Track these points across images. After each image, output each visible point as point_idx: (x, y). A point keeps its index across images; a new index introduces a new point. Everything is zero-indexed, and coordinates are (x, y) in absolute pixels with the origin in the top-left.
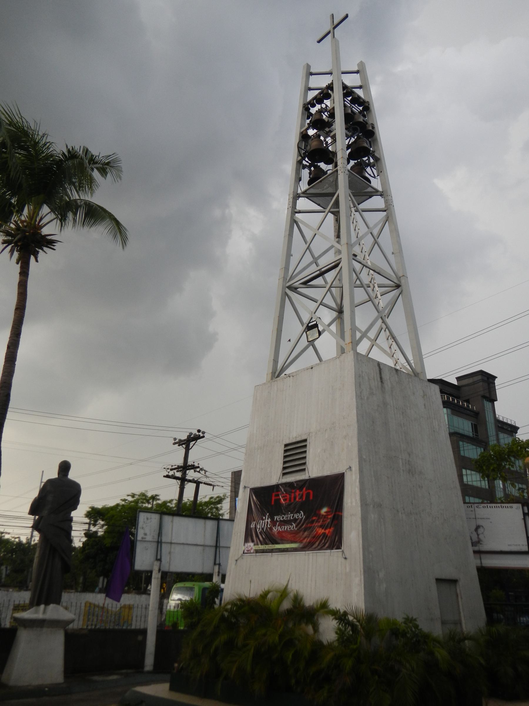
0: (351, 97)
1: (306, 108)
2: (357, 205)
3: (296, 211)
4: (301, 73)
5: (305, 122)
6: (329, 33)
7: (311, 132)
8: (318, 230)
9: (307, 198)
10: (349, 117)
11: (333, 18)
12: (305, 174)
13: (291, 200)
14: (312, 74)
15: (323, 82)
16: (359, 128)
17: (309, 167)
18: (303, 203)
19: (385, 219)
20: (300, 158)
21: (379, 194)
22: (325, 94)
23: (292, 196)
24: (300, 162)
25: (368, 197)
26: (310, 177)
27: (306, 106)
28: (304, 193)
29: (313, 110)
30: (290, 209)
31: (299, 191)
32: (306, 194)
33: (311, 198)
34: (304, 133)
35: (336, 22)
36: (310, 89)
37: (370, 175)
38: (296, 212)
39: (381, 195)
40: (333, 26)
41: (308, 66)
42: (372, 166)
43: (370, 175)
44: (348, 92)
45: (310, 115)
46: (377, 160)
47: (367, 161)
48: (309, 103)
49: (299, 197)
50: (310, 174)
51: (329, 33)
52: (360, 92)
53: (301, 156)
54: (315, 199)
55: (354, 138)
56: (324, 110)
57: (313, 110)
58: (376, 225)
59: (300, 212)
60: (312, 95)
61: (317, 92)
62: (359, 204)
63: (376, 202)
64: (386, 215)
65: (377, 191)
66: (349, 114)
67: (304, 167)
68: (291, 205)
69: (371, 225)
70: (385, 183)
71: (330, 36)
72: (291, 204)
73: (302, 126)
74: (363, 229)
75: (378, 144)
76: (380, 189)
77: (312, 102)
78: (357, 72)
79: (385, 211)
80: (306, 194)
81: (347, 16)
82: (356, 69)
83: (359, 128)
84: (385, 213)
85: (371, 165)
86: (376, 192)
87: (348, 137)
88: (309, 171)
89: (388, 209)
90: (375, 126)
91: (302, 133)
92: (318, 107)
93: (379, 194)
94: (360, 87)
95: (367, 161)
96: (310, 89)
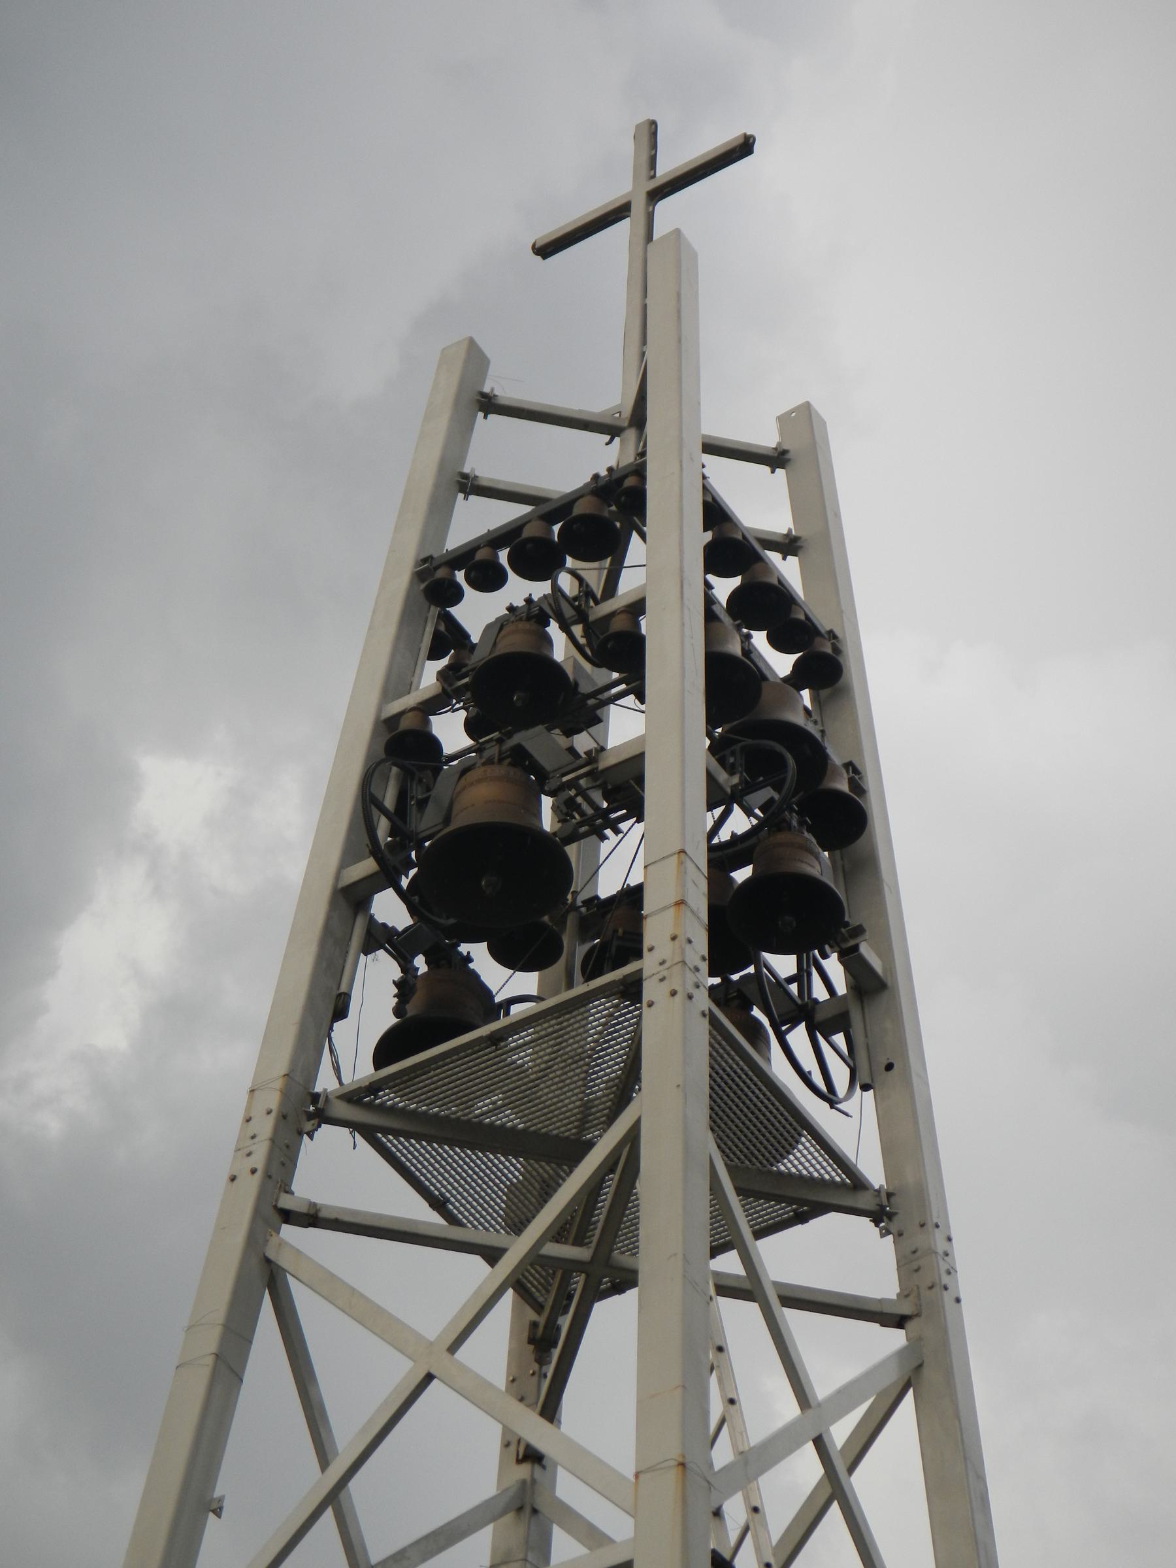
0: (736, 581)
1: (435, 585)
2: (747, 1232)
3: (285, 1202)
4: (429, 393)
5: (414, 669)
6: (619, 213)
7: (451, 731)
8: (454, 1348)
9: (368, 1133)
10: (730, 686)
11: (654, 145)
12: (376, 985)
13: (265, 1127)
14: (489, 405)
15: (569, 465)
16: (791, 761)
17: (400, 946)
18: (341, 1168)
19: (892, 1377)
20: (368, 866)
21: (864, 1201)
22: (606, 517)
23: (272, 1100)
24: (352, 899)
25: (786, 1211)
26: (398, 1011)
27: (441, 573)
28: (354, 1097)
29: (477, 612)
30: (250, 1187)
31: (325, 1082)
32: (374, 1115)
33: (389, 1141)
34: (405, 724)
35: (668, 165)
36: (470, 486)
37: (805, 1077)
38: (288, 1217)
39: (881, 1215)
40: (653, 185)
41: (475, 359)
42: (822, 1023)
43: (805, 1077)
44: (729, 547)
45: (449, 638)
46: (870, 985)
47: (794, 988)
48: (464, 558)
49: (322, 1117)
50: (404, 989)
51: (619, 213)
52: (789, 570)
53: (375, 851)
54: (408, 1149)
55: (749, 813)
56: (568, 612)
57: (477, 612)
58: (845, 1398)
59: (312, 1218)
60: (474, 520)
61: (509, 513)
62: (759, 1234)
63: (835, 1251)
64: (901, 1354)
65: (858, 1183)
66: (730, 659)
67: (379, 938)
68: (259, 1159)
69: (822, 1390)
70: (906, 1134)
71: (622, 229)
72: (261, 1151)
73: (398, 680)
74: (769, 1404)
75: (879, 892)
76: (874, 1173)
77: (480, 555)
78: (776, 459)
79: (899, 1322)
80: (370, 1106)
81: (744, 148)
82: (768, 439)
83: (791, 761)
84: (896, 1339)
85: (820, 1016)
86: (844, 1192)
87: (718, 797)
88: (397, 974)
89: (919, 1311)
90: (870, 784)
91: (391, 722)
92: (519, 590)
93: (864, 1201)
94: (789, 546)
95: (794, 988)
96: (470, 486)
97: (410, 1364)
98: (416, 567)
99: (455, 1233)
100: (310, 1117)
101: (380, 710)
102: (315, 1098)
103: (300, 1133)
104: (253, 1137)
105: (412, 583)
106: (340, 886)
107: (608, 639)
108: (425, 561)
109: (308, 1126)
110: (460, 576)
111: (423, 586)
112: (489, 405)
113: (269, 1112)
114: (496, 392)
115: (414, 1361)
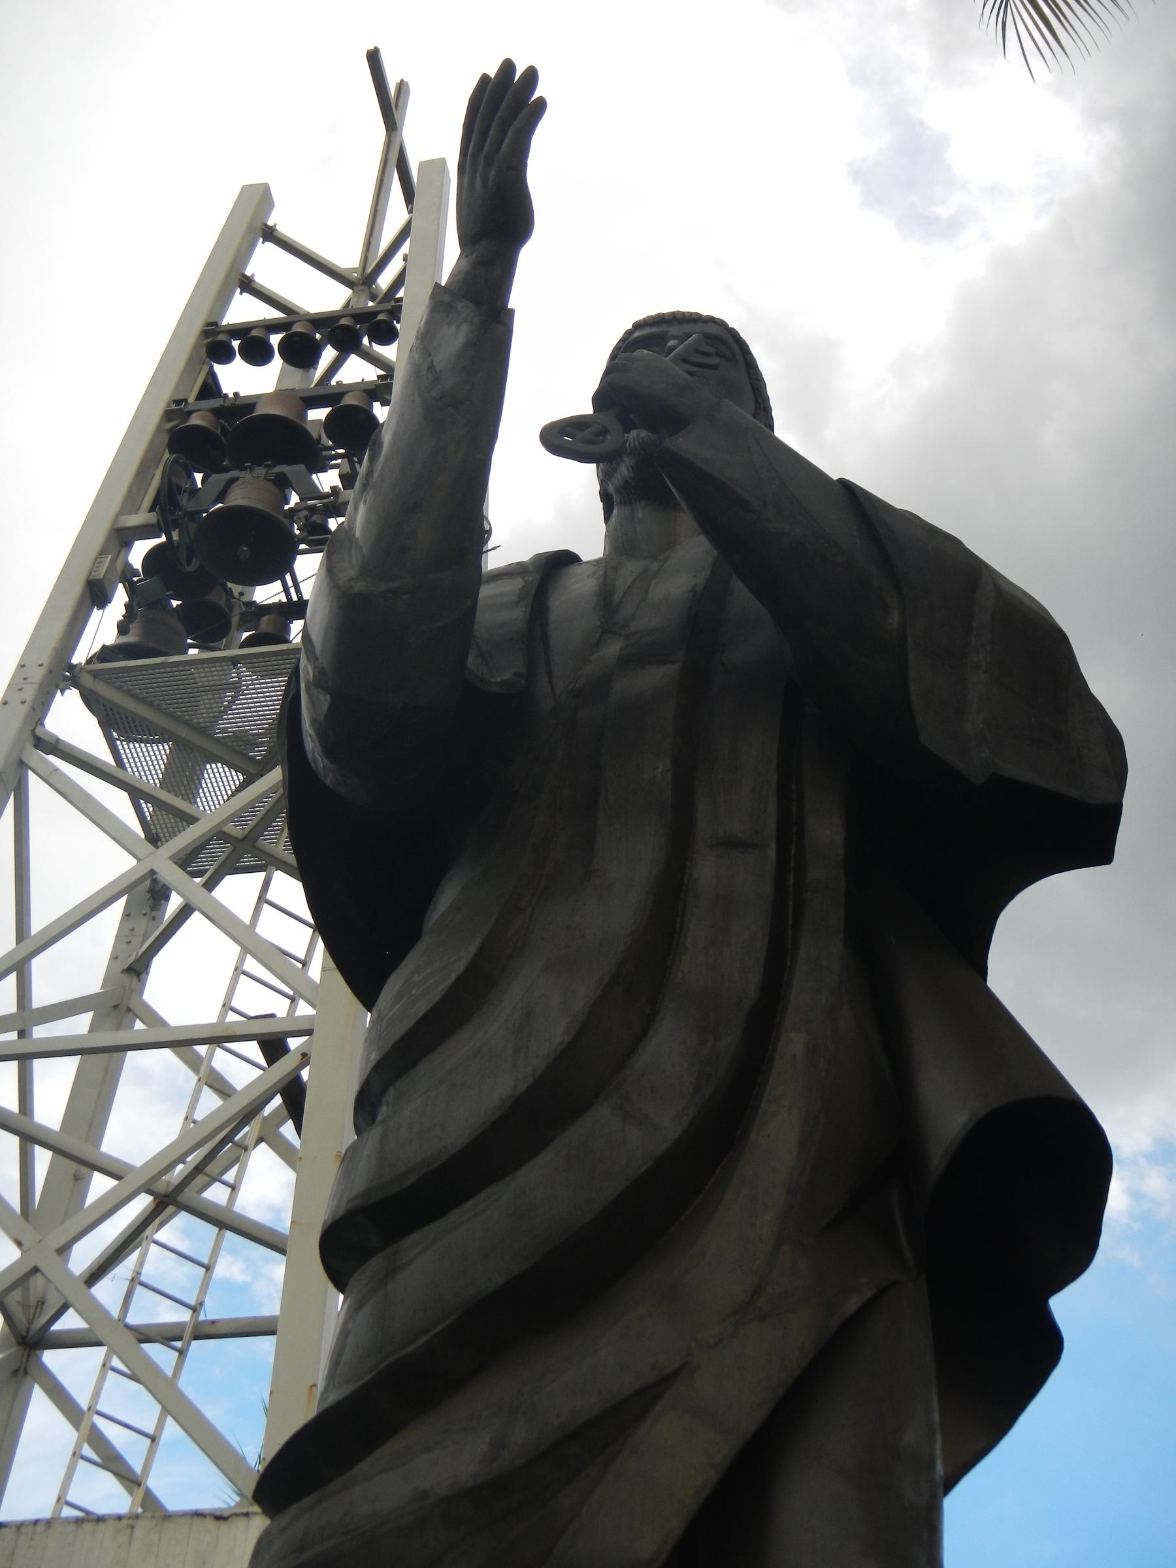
13: (37, 675)
14: (270, 235)
18: (72, 719)
27: (221, 337)
32: (104, 688)
36: (248, 285)
72: (30, 693)
96: (248, 285)
97: (134, 862)
98: (169, 405)
99: (119, 773)
100: (65, 679)
101: (116, 519)
102: (71, 667)
103: (57, 687)
104: (20, 690)
105: (199, 337)
106: (116, 526)
107: (269, 467)
108: (178, 402)
109: (62, 685)
110: (236, 344)
111: (206, 341)
112: (270, 235)
113: (23, 703)
114: (256, 279)
115: (139, 860)
